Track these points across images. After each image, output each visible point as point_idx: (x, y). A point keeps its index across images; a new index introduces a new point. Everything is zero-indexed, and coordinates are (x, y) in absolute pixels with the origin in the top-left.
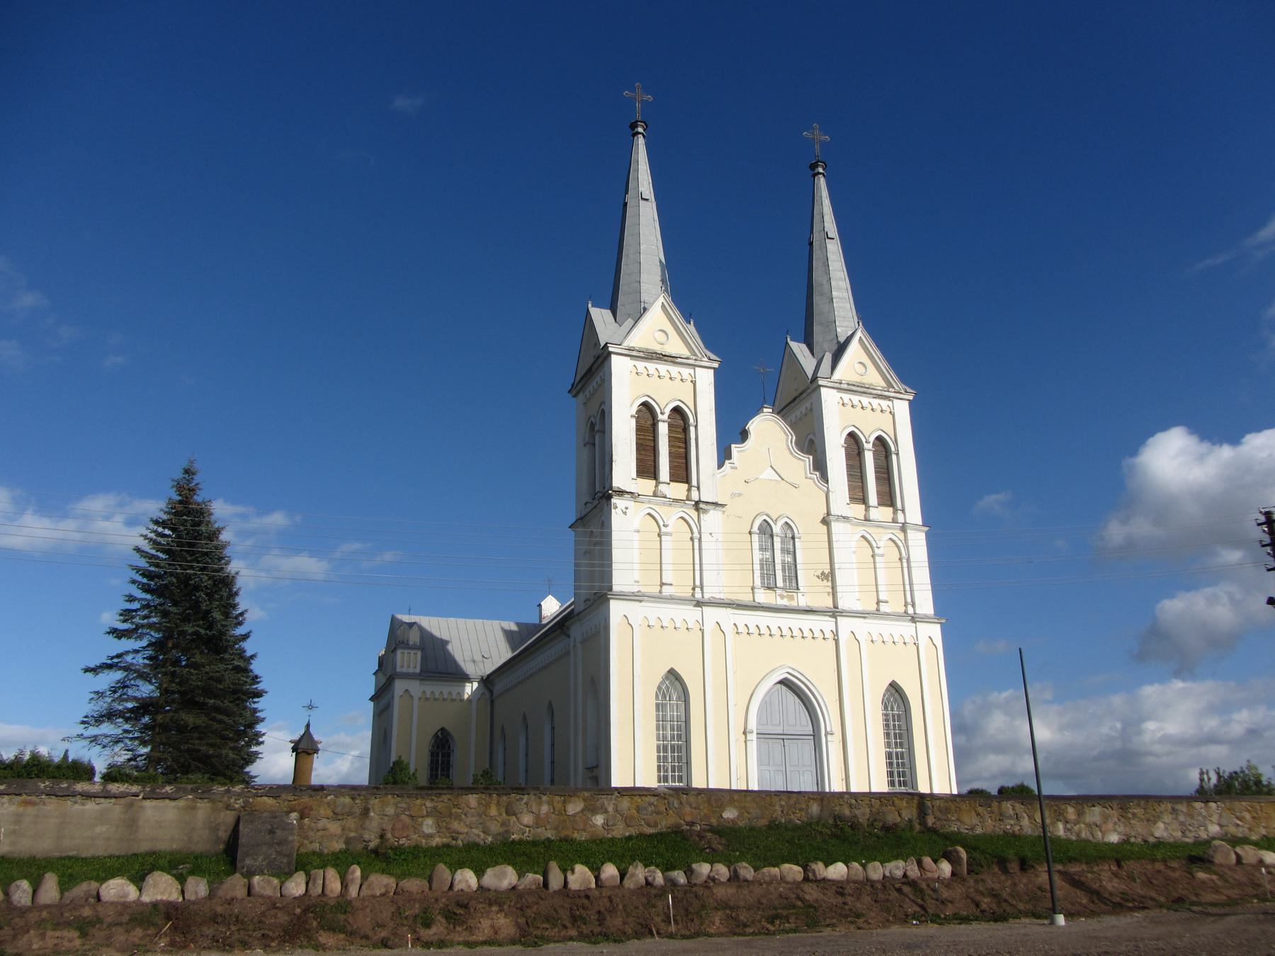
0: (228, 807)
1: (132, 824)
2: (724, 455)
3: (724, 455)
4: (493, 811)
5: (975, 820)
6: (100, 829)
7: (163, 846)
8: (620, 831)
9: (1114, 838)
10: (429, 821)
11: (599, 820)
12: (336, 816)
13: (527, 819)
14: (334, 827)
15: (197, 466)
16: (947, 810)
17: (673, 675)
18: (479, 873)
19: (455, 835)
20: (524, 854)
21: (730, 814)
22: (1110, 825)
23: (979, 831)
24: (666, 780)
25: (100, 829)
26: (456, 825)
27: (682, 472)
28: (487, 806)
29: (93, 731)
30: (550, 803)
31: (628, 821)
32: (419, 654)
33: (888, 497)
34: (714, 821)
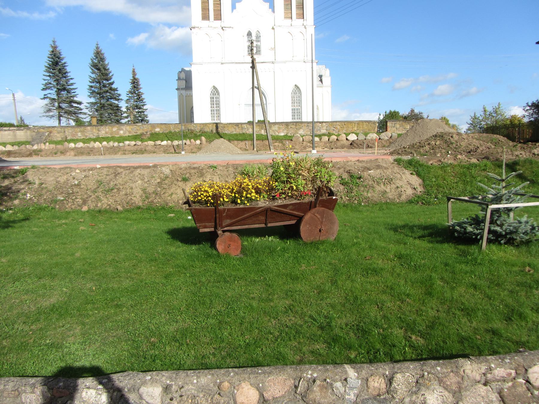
0: (34, 132)
1: (15, 136)
2: (234, 7)
3: (234, 7)
4: (94, 131)
5: (234, 130)
6: (9, 137)
7: (22, 140)
8: (127, 134)
9: (282, 134)
10: (79, 133)
11: (122, 132)
12: (58, 133)
13: (103, 132)
14: (58, 135)
15: (56, 40)
16: (224, 127)
17: (214, 87)
18: (75, 144)
19: (86, 136)
20: (84, 141)
21: (157, 130)
22: (281, 130)
23: (235, 133)
24: (295, 119)
25: (9, 137)
26: (86, 134)
27: (218, 17)
28: (93, 129)
29: (47, 114)
30: (108, 128)
31: (130, 132)
32: (184, 81)
33: (301, 15)
34: (153, 132)
